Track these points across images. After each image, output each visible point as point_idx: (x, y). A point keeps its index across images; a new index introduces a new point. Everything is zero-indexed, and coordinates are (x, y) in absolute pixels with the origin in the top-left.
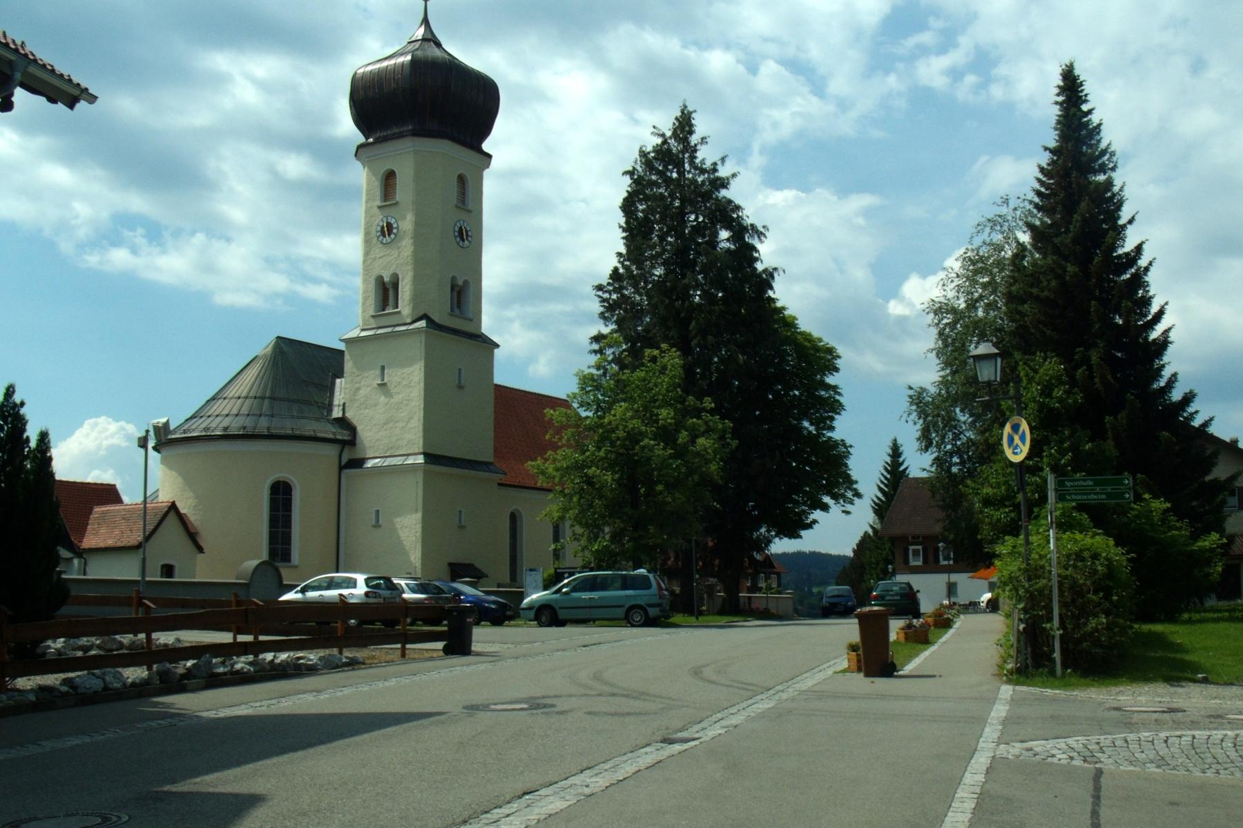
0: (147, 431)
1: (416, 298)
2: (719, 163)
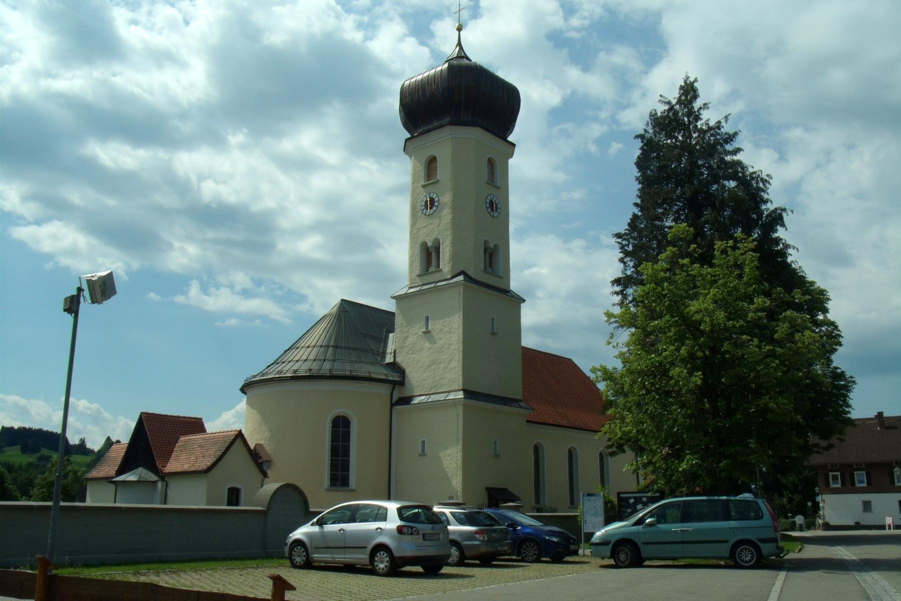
0: (80, 290)
1: (455, 258)
2: (723, 122)
